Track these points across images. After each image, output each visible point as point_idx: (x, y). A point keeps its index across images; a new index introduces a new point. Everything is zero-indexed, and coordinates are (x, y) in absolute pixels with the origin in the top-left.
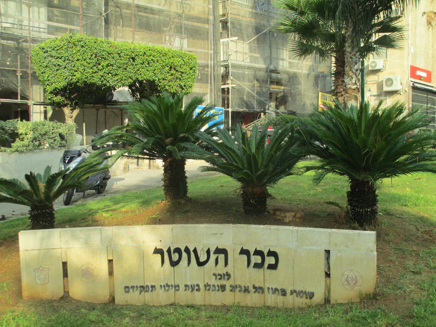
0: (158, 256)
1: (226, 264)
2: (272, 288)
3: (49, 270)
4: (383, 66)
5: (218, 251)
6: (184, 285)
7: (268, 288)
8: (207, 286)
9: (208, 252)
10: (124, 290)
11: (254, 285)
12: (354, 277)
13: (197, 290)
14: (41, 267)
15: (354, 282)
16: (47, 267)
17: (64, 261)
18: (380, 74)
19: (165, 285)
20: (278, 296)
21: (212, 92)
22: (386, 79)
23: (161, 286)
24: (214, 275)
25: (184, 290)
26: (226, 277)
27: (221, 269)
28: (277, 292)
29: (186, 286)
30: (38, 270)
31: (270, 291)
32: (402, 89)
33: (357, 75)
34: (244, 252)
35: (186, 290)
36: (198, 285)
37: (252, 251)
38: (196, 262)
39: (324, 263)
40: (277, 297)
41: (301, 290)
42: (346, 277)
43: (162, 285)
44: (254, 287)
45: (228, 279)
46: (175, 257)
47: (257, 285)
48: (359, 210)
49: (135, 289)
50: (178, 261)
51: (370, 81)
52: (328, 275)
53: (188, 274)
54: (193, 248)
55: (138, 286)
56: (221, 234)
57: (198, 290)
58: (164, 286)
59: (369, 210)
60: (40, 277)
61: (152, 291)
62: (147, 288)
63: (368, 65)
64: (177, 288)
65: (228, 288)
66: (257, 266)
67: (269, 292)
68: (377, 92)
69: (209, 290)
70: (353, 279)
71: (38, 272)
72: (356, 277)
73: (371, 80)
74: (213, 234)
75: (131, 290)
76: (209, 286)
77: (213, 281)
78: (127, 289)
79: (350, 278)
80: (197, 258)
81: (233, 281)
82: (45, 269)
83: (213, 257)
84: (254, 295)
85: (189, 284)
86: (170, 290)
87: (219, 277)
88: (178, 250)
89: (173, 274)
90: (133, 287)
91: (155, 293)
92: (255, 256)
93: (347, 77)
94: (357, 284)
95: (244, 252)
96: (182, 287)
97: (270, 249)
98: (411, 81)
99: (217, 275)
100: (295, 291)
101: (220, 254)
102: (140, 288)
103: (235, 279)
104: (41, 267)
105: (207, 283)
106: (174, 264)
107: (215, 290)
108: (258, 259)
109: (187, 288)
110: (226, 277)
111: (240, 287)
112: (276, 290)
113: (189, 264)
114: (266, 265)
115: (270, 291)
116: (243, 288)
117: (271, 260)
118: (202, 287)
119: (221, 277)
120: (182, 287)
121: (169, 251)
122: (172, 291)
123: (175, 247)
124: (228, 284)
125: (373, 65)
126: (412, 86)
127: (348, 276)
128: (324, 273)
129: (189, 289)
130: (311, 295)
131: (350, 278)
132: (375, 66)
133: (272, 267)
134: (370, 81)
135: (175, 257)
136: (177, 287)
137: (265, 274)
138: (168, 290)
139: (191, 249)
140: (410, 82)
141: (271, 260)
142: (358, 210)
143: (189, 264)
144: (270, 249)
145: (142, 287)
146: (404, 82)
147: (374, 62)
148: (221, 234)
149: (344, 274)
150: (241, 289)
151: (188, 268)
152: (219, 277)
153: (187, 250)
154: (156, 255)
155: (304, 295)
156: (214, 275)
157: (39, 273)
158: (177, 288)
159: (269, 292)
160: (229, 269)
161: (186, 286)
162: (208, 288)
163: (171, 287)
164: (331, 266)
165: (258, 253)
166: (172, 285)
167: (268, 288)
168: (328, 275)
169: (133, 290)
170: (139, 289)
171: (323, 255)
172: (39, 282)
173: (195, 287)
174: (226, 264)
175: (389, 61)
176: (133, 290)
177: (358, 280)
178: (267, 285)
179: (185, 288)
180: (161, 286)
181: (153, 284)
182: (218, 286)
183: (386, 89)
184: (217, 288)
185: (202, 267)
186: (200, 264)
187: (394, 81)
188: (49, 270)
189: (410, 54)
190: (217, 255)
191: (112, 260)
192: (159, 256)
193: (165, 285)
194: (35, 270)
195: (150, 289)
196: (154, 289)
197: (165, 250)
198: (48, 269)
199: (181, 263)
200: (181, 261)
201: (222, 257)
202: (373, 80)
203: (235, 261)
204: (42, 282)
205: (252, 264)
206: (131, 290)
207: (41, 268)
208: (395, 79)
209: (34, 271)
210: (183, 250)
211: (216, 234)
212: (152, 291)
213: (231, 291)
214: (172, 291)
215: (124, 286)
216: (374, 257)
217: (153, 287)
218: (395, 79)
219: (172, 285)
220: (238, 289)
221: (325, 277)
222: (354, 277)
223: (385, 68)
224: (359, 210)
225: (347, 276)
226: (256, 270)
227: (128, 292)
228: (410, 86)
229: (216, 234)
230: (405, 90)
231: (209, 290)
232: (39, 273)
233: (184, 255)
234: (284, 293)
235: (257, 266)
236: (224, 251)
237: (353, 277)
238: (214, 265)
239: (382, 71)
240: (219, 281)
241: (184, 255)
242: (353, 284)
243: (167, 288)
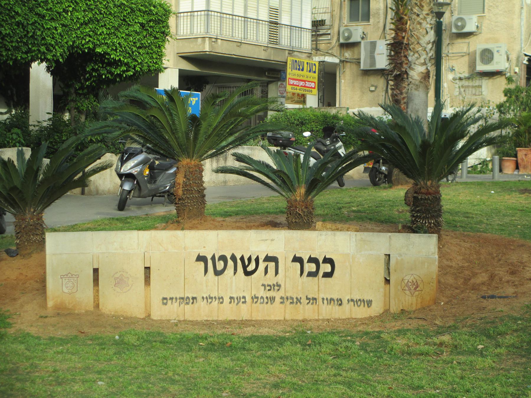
0: (200, 264)
1: (277, 273)
2: (327, 299)
3: (77, 277)
4: (477, 27)
5: (268, 259)
6: (229, 297)
7: (323, 299)
8: (255, 298)
9: (257, 260)
10: (161, 302)
11: (307, 297)
12: (415, 281)
13: (243, 302)
14: (69, 273)
15: (414, 287)
16: (76, 274)
17: (96, 267)
18: (472, 40)
19: (208, 297)
20: (334, 307)
21: (219, 76)
22: (481, 50)
23: (203, 298)
24: (263, 285)
25: (228, 302)
26: (276, 288)
27: (271, 279)
28: (332, 302)
29: (231, 298)
30: (65, 276)
31: (325, 302)
32: (508, 69)
33: (428, 50)
34: (297, 259)
35: (230, 302)
36: (244, 297)
37: (306, 259)
38: (243, 271)
39: (383, 269)
40: (332, 308)
41: (358, 298)
42: (406, 281)
43: (205, 297)
44: (307, 298)
45: (278, 290)
46: (220, 265)
47: (310, 296)
48: (421, 222)
49: (174, 300)
50: (222, 270)
51: (453, 53)
52: (387, 281)
53: (234, 284)
54: (241, 256)
55: (178, 297)
56: (272, 240)
57: (244, 302)
58: (207, 298)
59: (432, 222)
60: (68, 285)
61: (193, 303)
62: (188, 300)
63: (450, 23)
64: (221, 300)
65: (278, 300)
66: (310, 274)
67: (323, 303)
68: (469, 73)
69: (256, 302)
70: (414, 284)
71: (65, 280)
72: (416, 282)
73: (455, 51)
74: (262, 240)
75: (169, 302)
76: (257, 298)
77: (262, 293)
78: (165, 301)
79: (411, 282)
80: (245, 267)
81: (284, 292)
82: (74, 276)
83: (262, 265)
84: (307, 307)
85: (235, 296)
86: (213, 303)
87: (268, 288)
88: (223, 258)
89: (217, 284)
90: (172, 299)
91: (196, 305)
92: (310, 264)
93: (412, 53)
94: (417, 289)
95: (297, 259)
96: (227, 300)
97: (325, 256)
98: (526, 55)
99: (266, 286)
100: (352, 300)
101: (270, 263)
102: (179, 299)
103: (286, 290)
104: (69, 273)
105: (255, 295)
106: (218, 273)
107: (263, 303)
108: (312, 267)
109: (232, 300)
110: (276, 288)
111: (292, 298)
112: (332, 299)
113: (235, 273)
114: (321, 273)
115: (325, 302)
116: (295, 300)
117: (327, 268)
118: (248, 299)
119: (271, 287)
120: (227, 300)
121: (213, 258)
122: (215, 303)
123: (220, 255)
124: (277, 295)
125: (459, 24)
126: (527, 63)
127: (408, 281)
128: (383, 279)
129: (234, 302)
130: (369, 303)
131: (411, 282)
132: (463, 27)
133: (328, 275)
134: (453, 53)
135: (220, 265)
136: (221, 299)
137: (320, 284)
138: (211, 302)
139: (238, 257)
140: (524, 56)
141: (327, 268)
142: (420, 221)
143: (235, 273)
144: (325, 256)
145: (183, 298)
146: (513, 57)
147: (461, 19)
148: (272, 240)
149: (405, 278)
150: (293, 301)
151: (234, 277)
152: (268, 288)
153: (233, 258)
154: (199, 263)
155: (362, 303)
156: (263, 285)
157: (67, 281)
158: (221, 300)
159: (323, 303)
160: (280, 278)
161: (231, 298)
162: (255, 300)
163: (214, 300)
164: (391, 271)
165: (312, 260)
166: (215, 298)
167: (323, 299)
168: (387, 281)
169: (172, 302)
170: (178, 301)
171: (383, 257)
172: (65, 290)
173: (241, 299)
174: (277, 273)
175: (487, 17)
176: (172, 302)
177: (419, 284)
178: (322, 296)
179: (230, 300)
180: (203, 298)
181: (194, 296)
182: (267, 298)
183: (481, 67)
184: (266, 300)
185: (250, 277)
186: (248, 274)
187: (496, 55)
188: (77, 277)
189: (525, 7)
190: (266, 263)
191: (149, 268)
192: (202, 264)
193: (208, 297)
194: (62, 277)
195: (191, 301)
196: (195, 300)
197: (209, 257)
198: (77, 276)
199: (226, 272)
200: (226, 270)
201: (272, 265)
202: (458, 51)
203: (286, 269)
204: (70, 291)
205: (305, 273)
206: (169, 302)
207: (70, 275)
208: (498, 51)
209: (61, 278)
210: (229, 258)
211: (266, 240)
212: (193, 303)
213: (281, 303)
214: (215, 303)
215: (161, 298)
216: (435, 260)
217: (193, 298)
218: (498, 51)
219: (215, 298)
220: (290, 301)
221: (385, 284)
222: (415, 281)
223: (480, 31)
224: (421, 222)
225: (407, 280)
226: (310, 278)
227: (166, 304)
228: (522, 63)
229: (266, 240)
230: (514, 70)
231: (256, 302)
232: (67, 281)
233: (230, 263)
234: (340, 302)
235: (310, 274)
236: (274, 260)
237: (413, 282)
238: (264, 274)
239: (476, 35)
240: (268, 292)
241: (230, 263)
242: (413, 289)
243: (210, 300)
